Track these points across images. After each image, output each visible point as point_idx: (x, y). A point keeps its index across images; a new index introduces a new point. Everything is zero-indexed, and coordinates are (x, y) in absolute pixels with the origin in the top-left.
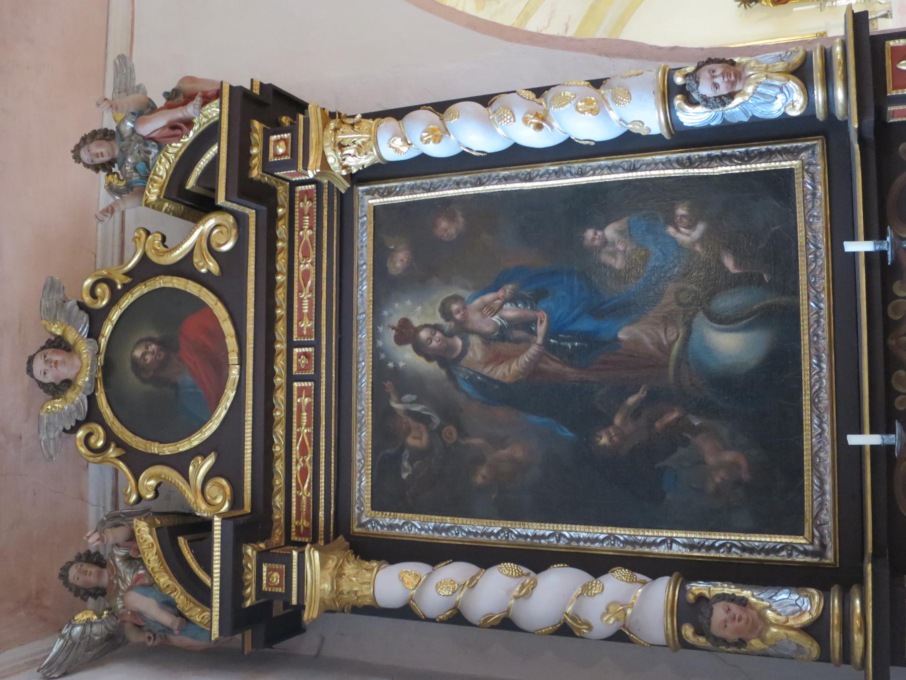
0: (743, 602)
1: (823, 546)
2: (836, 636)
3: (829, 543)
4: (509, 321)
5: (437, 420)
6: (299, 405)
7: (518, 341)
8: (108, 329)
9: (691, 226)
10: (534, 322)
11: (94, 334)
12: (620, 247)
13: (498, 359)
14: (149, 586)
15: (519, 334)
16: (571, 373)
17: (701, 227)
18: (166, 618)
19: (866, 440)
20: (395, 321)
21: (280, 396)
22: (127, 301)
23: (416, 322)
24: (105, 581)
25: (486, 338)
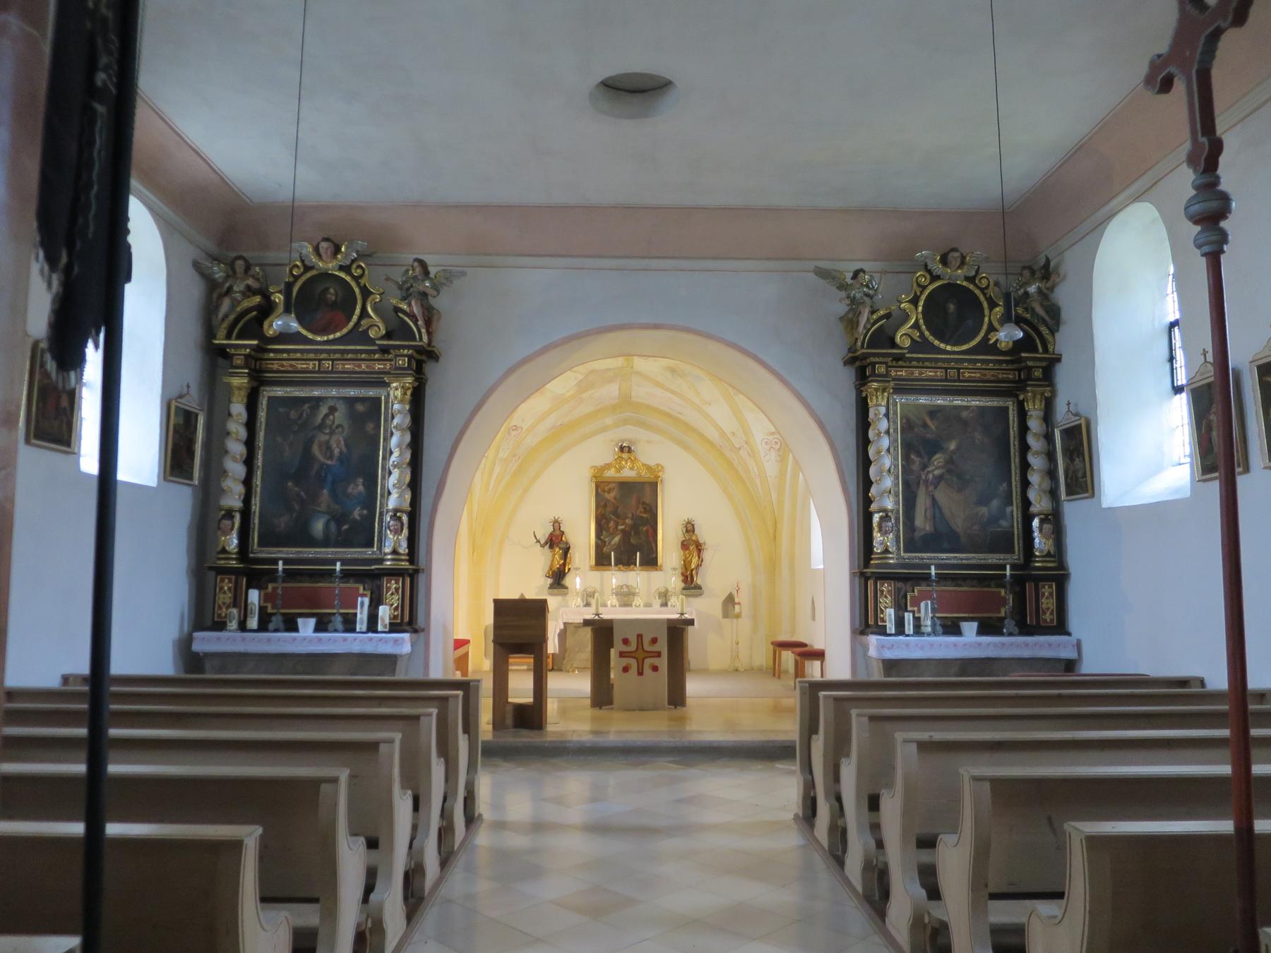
0: (232, 529)
1: (255, 553)
2: (223, 556)
3: (256, 555)
4: (333, 450)
5: (300, 422)
6: (309, 364)
7: (326, 453)
8: (342, 275)
9: (360, 515)
10: (332, 460)
11: (341, 268)
12: (355, 491)
13: (320, 446)
14: (233, 307)
15: (328, 454)
16: (313, 473)
17: (358, 518)
18: (221, 315)
19: (1008, 572)
20: (338, 406)
21: (312, 356)
22: (353, 284)
23: (336, 414)
24: (239, 275)
25: (328, 442)
